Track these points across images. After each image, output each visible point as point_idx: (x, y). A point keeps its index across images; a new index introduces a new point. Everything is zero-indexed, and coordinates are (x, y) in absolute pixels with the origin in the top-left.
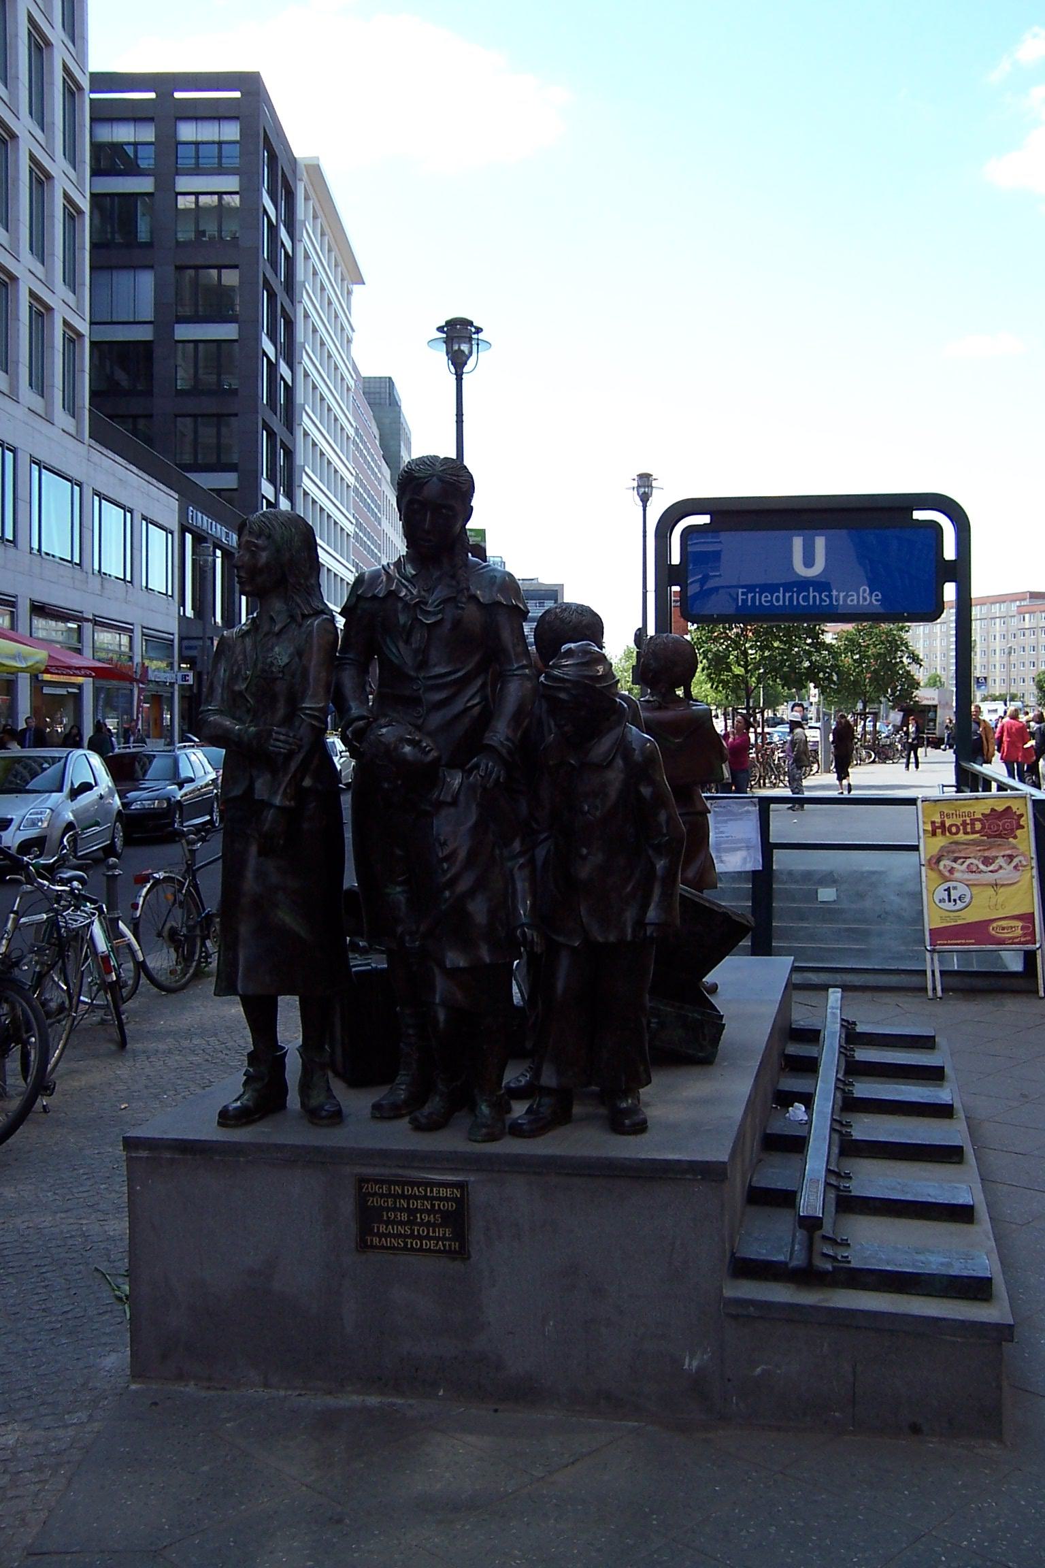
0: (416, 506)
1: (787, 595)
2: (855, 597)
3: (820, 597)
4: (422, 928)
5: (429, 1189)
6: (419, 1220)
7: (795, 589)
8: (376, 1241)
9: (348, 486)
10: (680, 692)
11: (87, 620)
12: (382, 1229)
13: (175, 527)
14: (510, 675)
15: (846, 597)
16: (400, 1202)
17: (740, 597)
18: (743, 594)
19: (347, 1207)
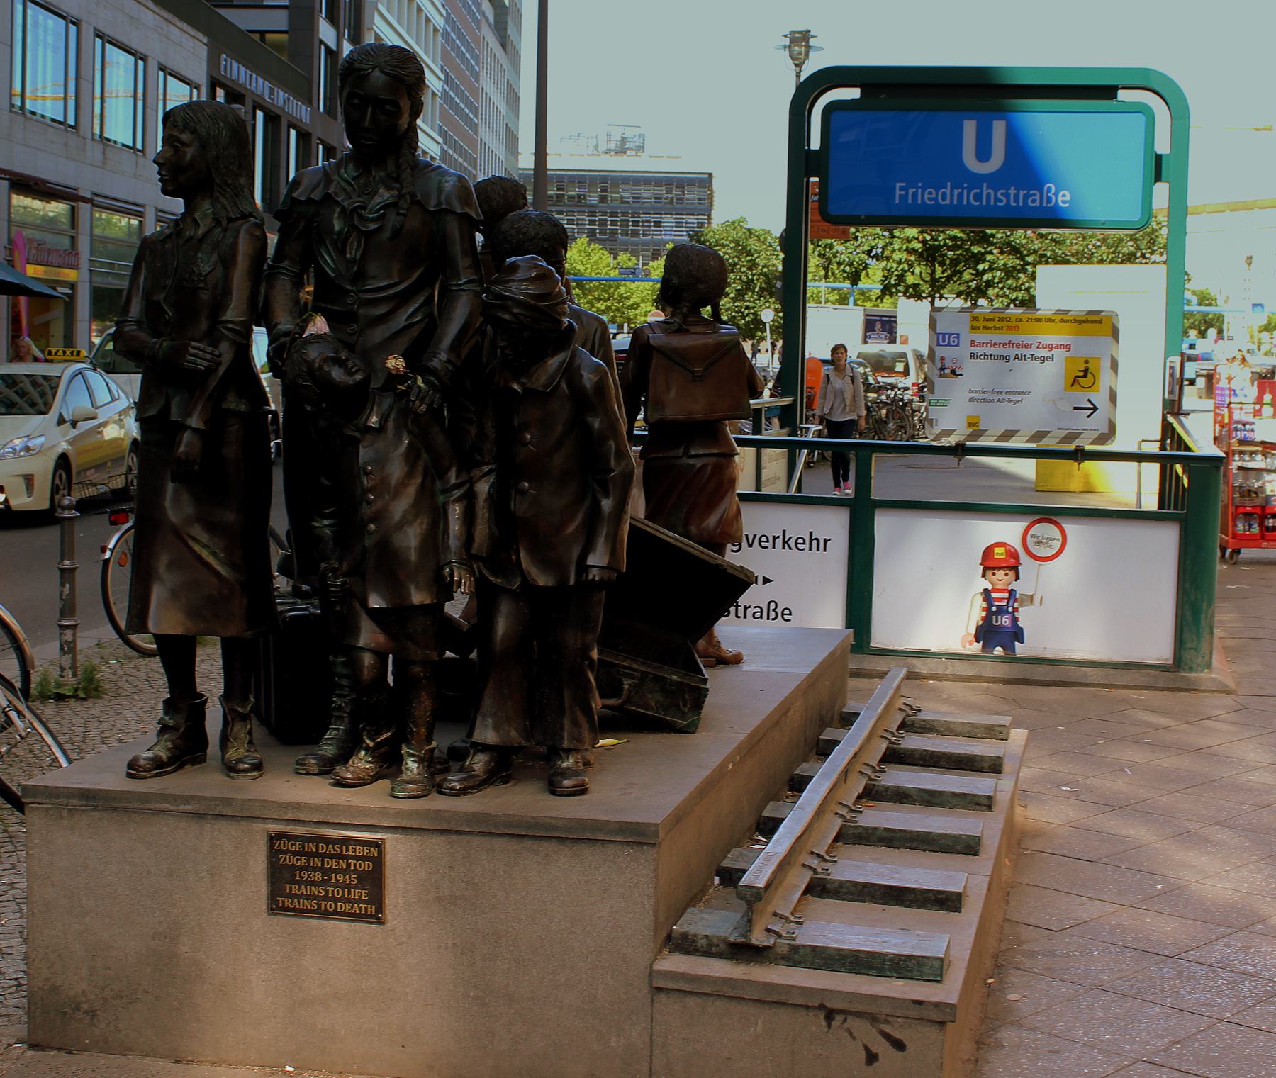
0: (356, 101)
1: (956, 192)
2: (1037, 198)
3: (995, 195)
4: (345, 567)
5: (344, 847)
6: (333, 881)
7: (920, 184)
8: (288, 902)
9: (436, 30)
10: (707, 311)
11: (86, 200)
12: (295, 889)
13: (203, 80)
14: (457, 290)
15: (1026, 197)
16: (314, 860)
17: (898, 193)
18: (901, 189)
19: (258, 864)
